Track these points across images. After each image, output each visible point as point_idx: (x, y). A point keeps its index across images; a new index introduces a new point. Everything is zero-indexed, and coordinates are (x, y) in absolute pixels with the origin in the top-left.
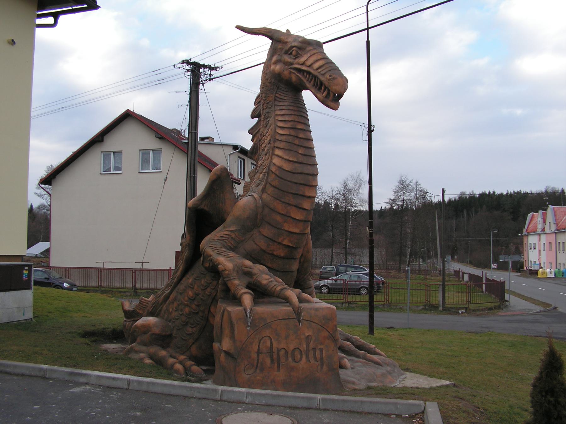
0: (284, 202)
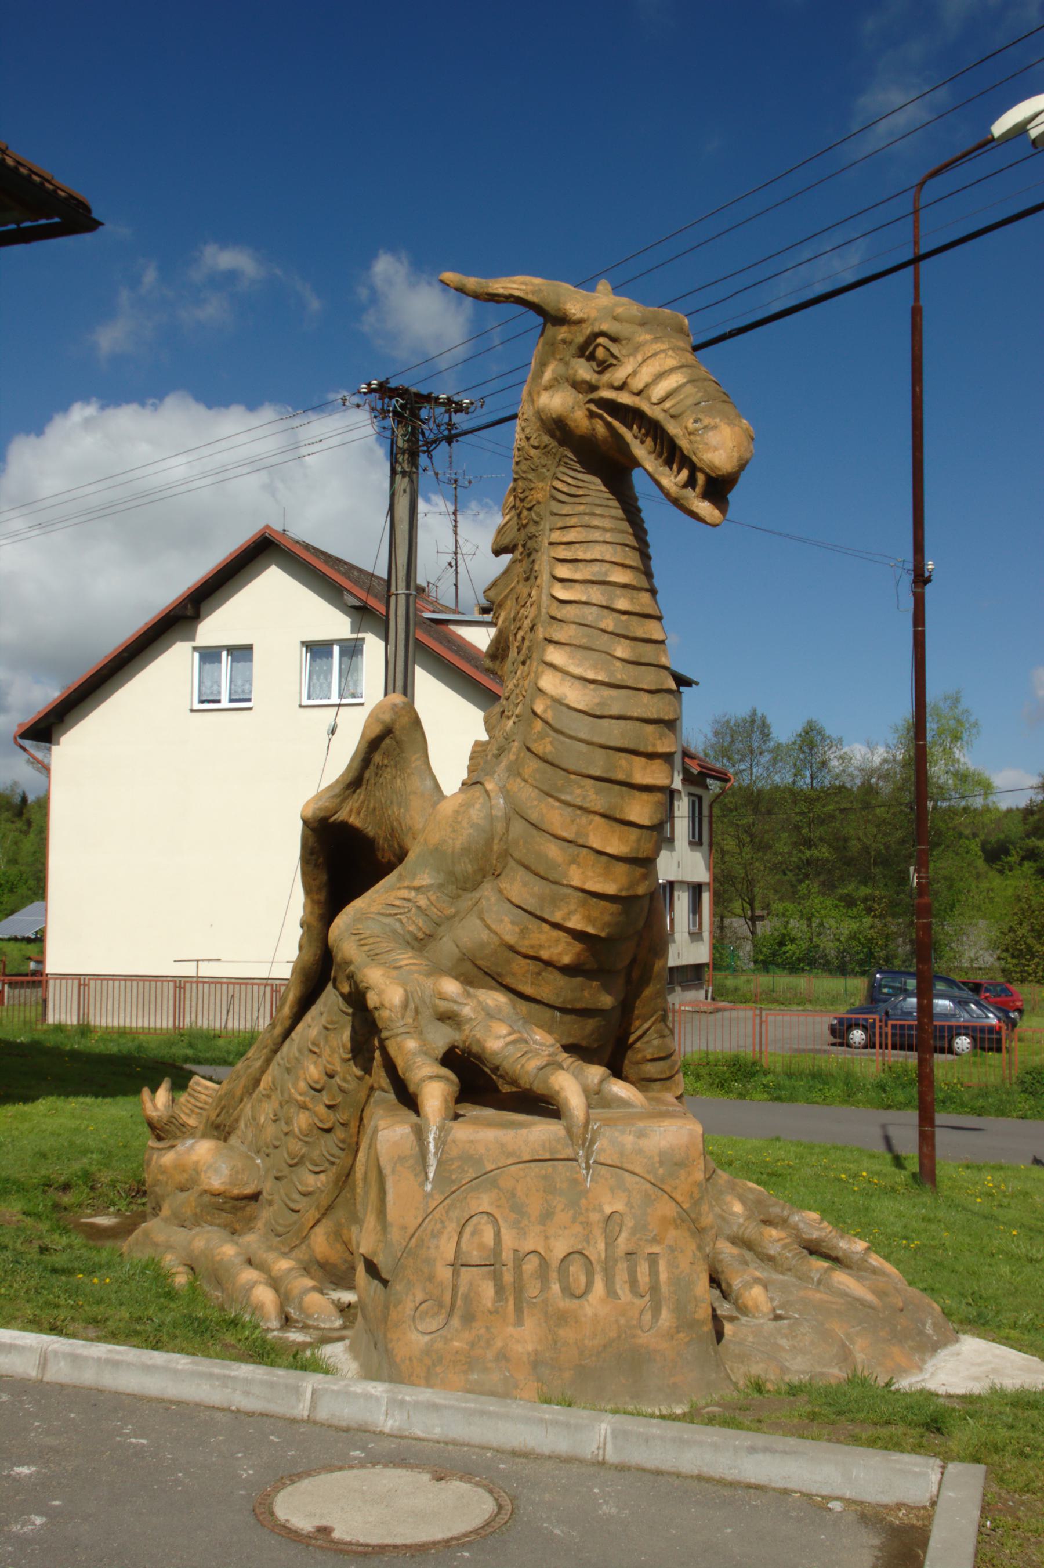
0: (568, 804)
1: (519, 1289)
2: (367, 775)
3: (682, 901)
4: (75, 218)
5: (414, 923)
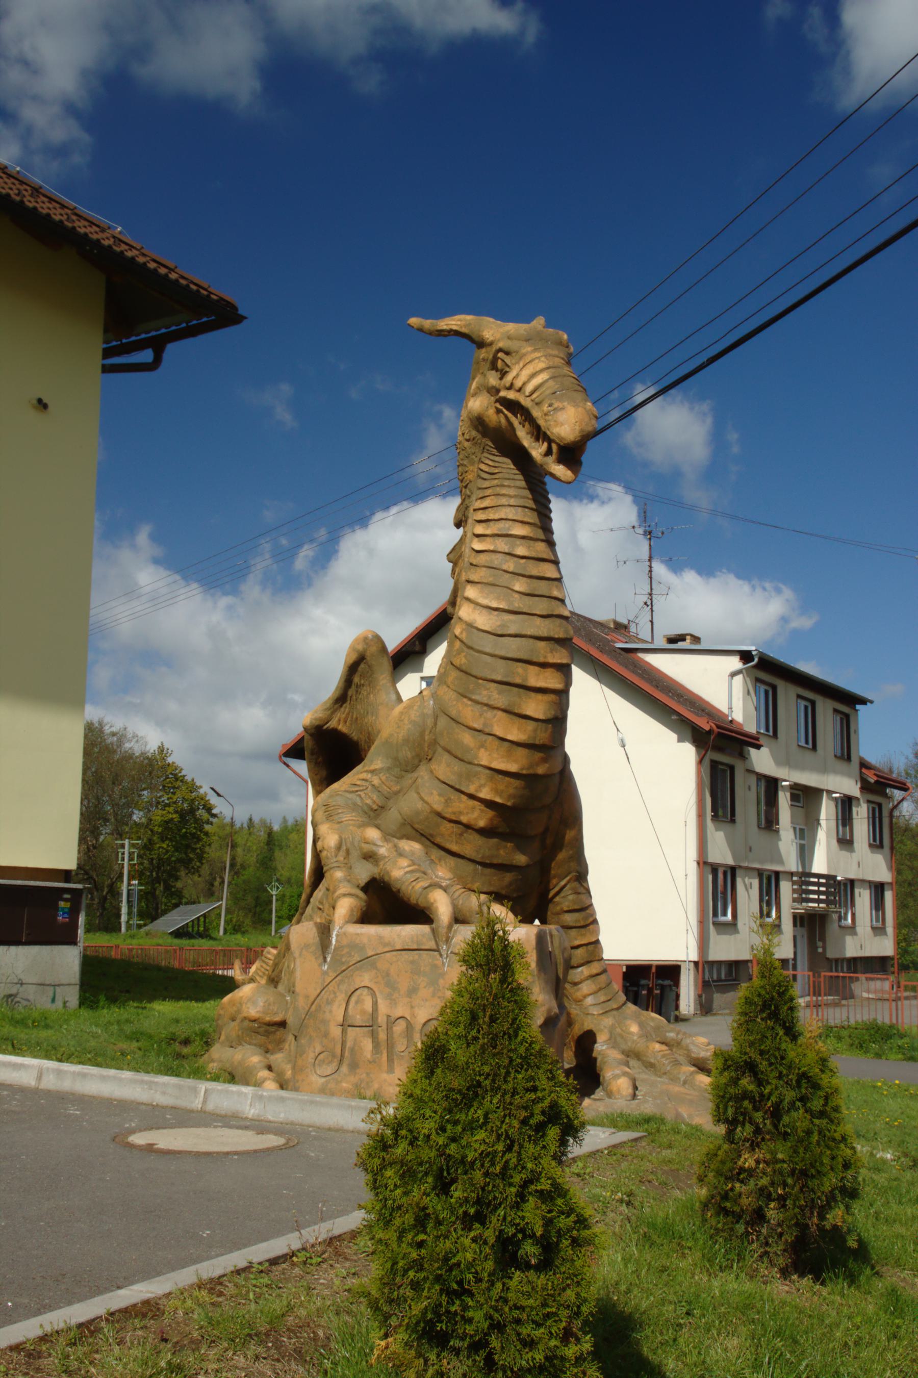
0: (477, 702)
1: (390, 1046)
2: (350, 693)
3: (863, 898)
4: (224, 315)
5: (370, 797)
